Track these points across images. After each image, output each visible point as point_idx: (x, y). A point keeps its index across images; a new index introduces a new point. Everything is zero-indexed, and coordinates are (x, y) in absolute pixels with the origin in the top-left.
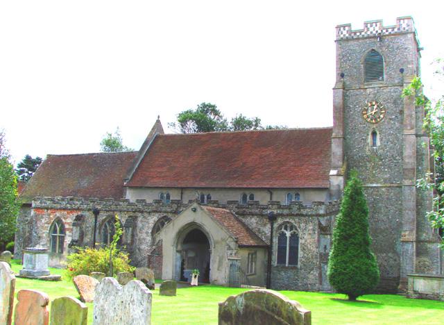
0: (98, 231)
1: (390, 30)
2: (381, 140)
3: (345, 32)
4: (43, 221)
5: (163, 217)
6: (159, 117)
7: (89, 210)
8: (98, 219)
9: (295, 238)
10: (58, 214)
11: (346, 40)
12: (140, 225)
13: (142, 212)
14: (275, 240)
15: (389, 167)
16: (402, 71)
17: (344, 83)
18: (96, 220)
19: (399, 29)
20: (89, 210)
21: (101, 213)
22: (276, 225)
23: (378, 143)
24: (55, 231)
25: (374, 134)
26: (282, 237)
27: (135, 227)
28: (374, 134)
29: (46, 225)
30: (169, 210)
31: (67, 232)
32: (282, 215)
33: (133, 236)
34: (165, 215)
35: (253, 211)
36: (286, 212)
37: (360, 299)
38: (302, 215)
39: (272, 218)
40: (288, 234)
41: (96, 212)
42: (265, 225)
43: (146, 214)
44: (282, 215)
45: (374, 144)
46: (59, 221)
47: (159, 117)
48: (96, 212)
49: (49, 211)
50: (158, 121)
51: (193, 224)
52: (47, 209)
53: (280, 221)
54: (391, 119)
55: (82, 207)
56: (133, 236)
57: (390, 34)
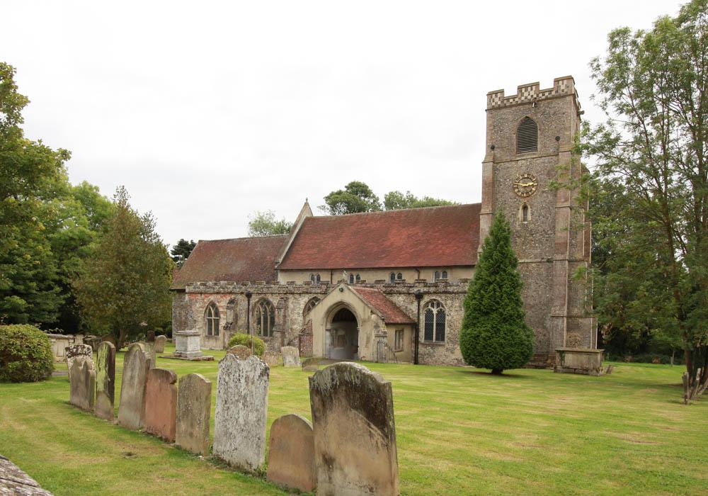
0: (251, 313)
1: (547, 94)
2: (532, 214)
3: (497, 100)
4: (198, 305)
5: (314, 298)
6: (307, 200)
7: (242, 293)
8: (251, 302)
9: (441, 314)
10: (212, 298)
11: (498, 106)
12: (291, 306)
13: (293, 294)
14: (422, 318)
15: (541, 242)
16: (558, 139)
17: (494, 156)
18: (249, 303)
19: (557, 92)
20: (242, 293)
21: (253, 296)
22: (422, 303)
23: (529, 217)
24: (210, 314)
25: (525, 208)
26: (429, 314)
27: (286, 308)
28: (525, 208)
29: (201, 309)
30: (319, 291)
31: (222, 316)
32: (428, 293)
33: (285, 316)
34: (315, 295)
35: (400, 289)
36: (432, 289)
37: (505, 372)
38: (450, 293)
39: (419, 297)
40: (435, 311)
41: (249, 295)
42: (412, 303)
43: (297, 296)
44: (428, 293)
45: (525, 219)
46: (213, 305)
47: (307, 200)
48: (249, 295)
49: (203, 296)
50: (306, 204)
51: (341, 303)
52: (201, 294)
53: (426, 299)
54: (543, 192)
55: (235, 290)
56: (285, 316)
57: (547, 99)
